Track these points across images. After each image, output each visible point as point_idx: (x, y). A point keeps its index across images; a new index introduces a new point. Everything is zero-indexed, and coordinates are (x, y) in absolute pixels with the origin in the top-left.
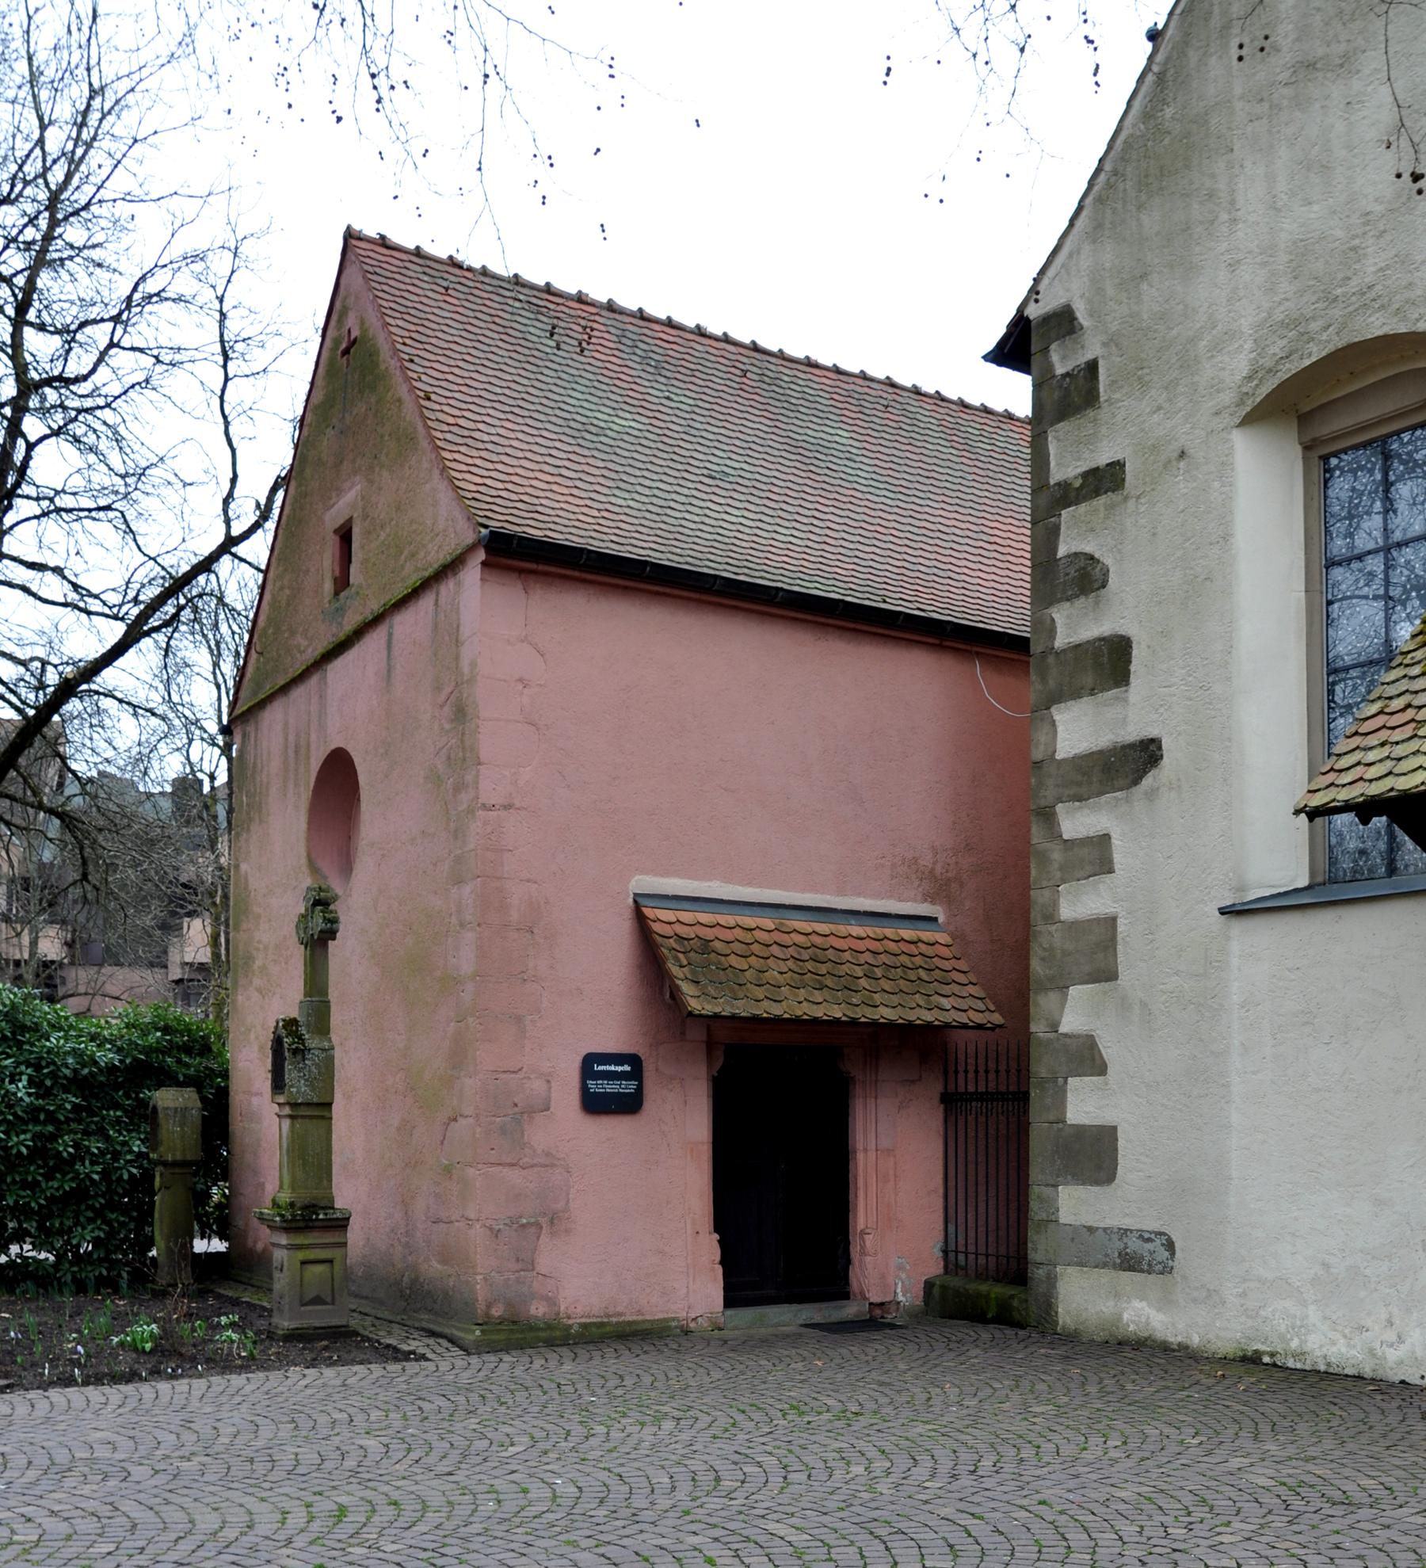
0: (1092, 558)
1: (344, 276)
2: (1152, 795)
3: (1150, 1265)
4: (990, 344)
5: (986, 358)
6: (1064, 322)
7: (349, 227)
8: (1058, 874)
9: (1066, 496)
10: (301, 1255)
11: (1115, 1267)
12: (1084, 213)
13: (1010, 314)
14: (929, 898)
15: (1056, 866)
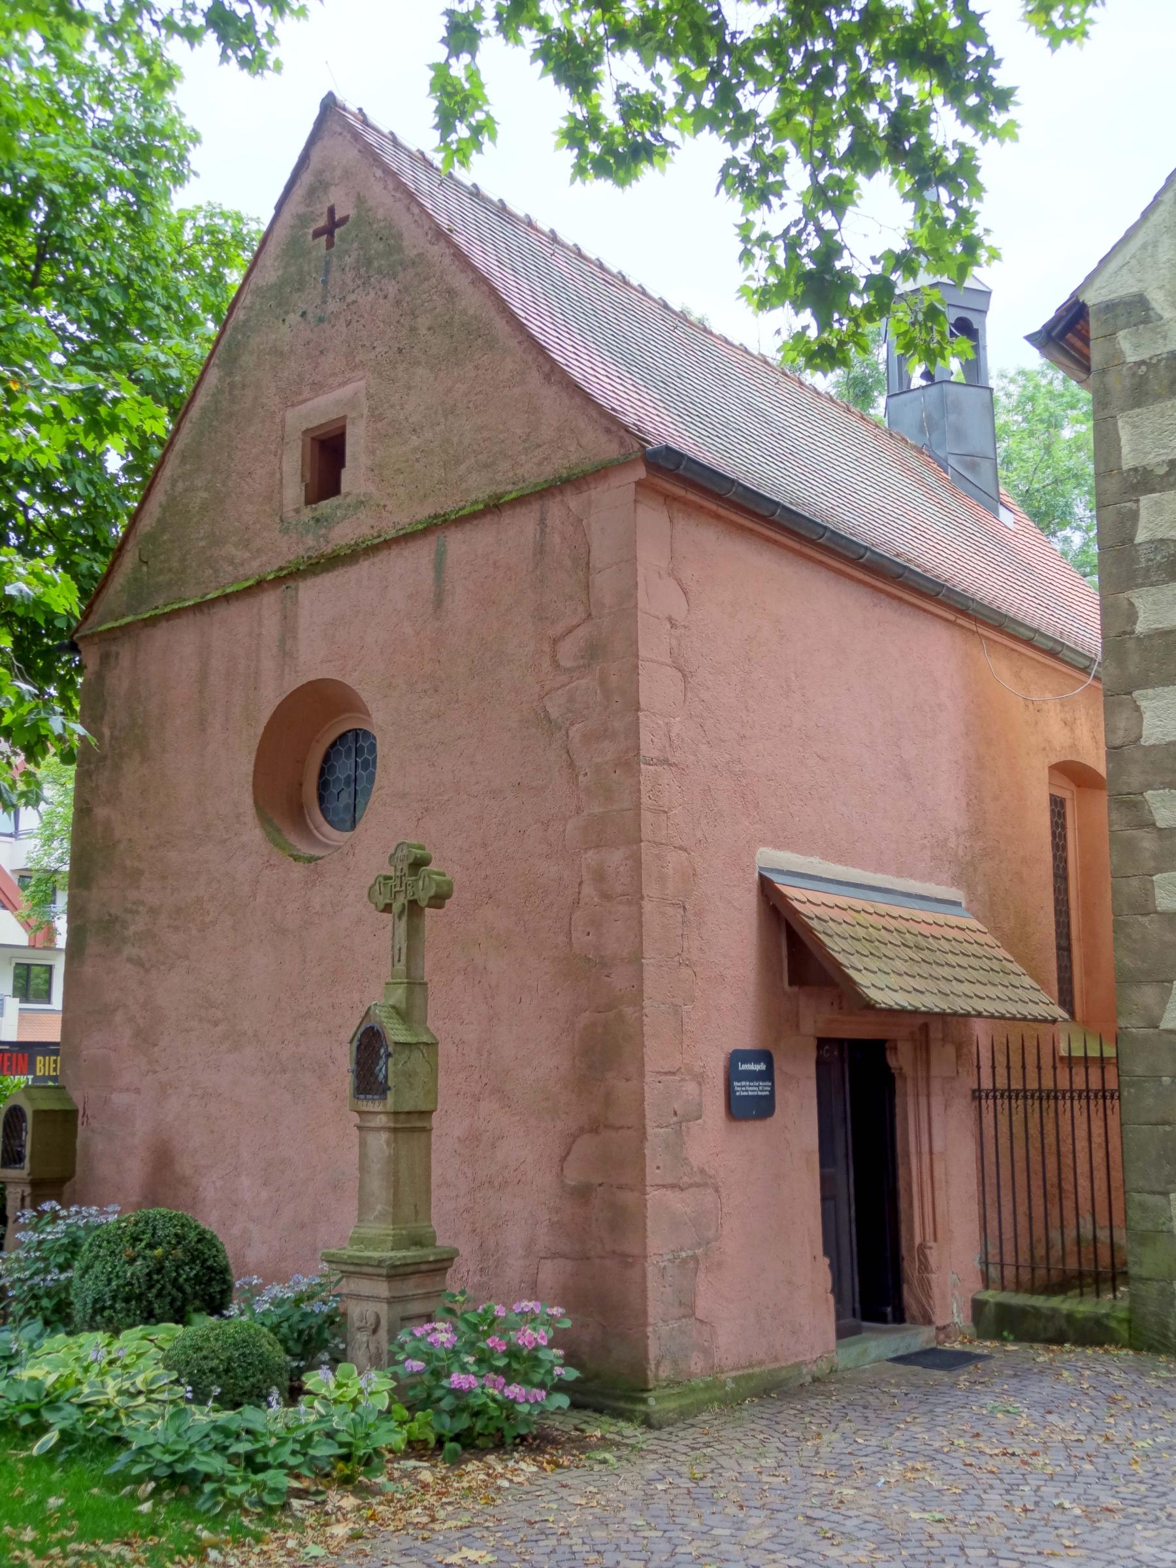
1: (319, 145)
4: (1036, 326)
5: (1029, 338)
6: (1135, 310)
7: (331, 95)
8: (1152, 864)
9: (1143, 482)
10: (400, 1310)
12: (1162, 208)
13: (1062, 297)
14: (956, 881)
15: (1147, 855)
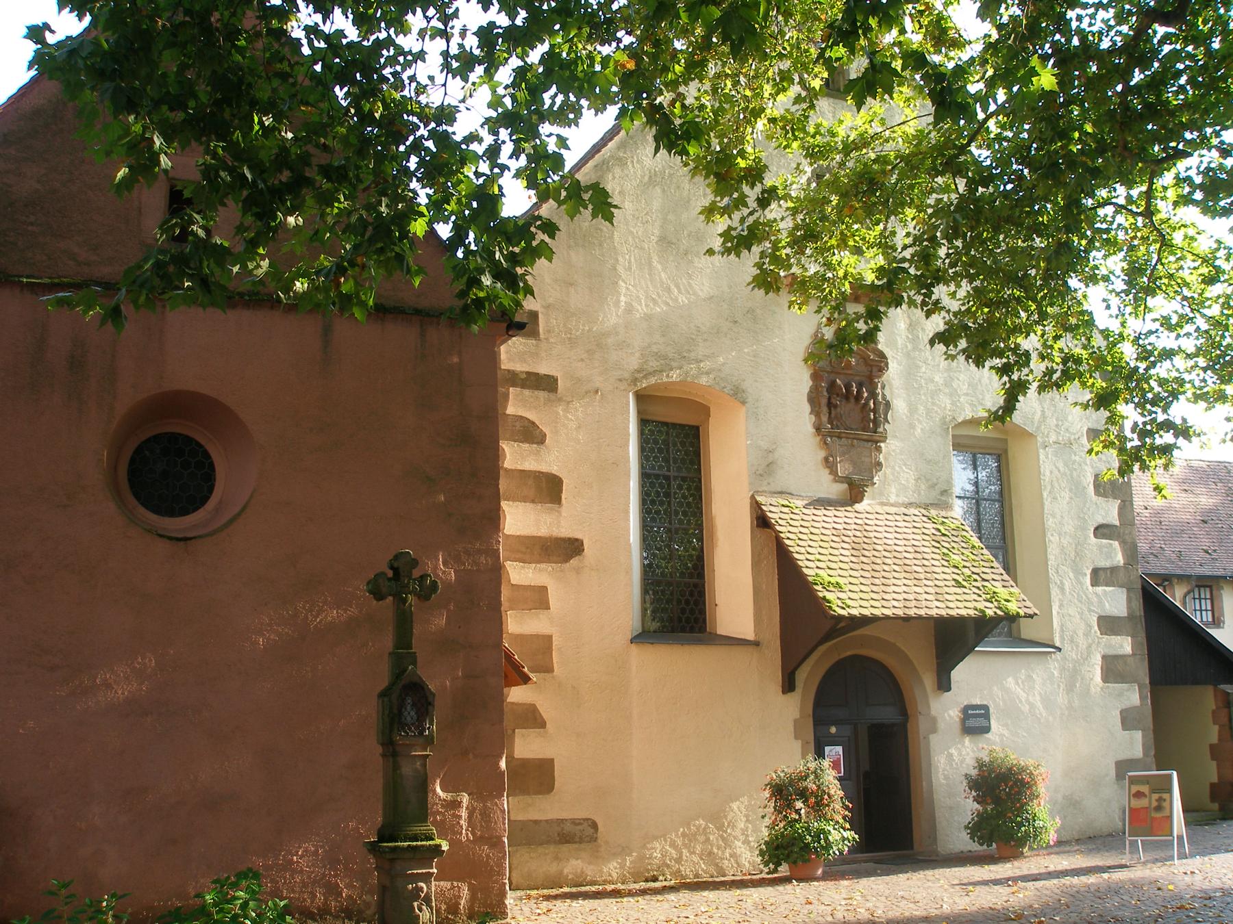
0: (533, 423)
2: (578, 571)
3: (581, 838)
4: (56, 7)
11: (555, 843)
